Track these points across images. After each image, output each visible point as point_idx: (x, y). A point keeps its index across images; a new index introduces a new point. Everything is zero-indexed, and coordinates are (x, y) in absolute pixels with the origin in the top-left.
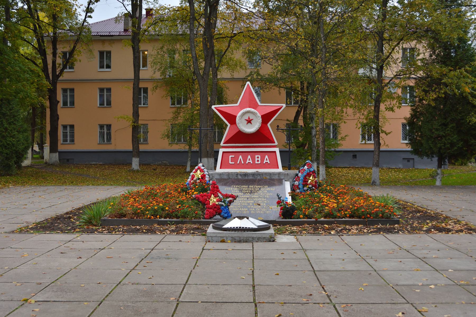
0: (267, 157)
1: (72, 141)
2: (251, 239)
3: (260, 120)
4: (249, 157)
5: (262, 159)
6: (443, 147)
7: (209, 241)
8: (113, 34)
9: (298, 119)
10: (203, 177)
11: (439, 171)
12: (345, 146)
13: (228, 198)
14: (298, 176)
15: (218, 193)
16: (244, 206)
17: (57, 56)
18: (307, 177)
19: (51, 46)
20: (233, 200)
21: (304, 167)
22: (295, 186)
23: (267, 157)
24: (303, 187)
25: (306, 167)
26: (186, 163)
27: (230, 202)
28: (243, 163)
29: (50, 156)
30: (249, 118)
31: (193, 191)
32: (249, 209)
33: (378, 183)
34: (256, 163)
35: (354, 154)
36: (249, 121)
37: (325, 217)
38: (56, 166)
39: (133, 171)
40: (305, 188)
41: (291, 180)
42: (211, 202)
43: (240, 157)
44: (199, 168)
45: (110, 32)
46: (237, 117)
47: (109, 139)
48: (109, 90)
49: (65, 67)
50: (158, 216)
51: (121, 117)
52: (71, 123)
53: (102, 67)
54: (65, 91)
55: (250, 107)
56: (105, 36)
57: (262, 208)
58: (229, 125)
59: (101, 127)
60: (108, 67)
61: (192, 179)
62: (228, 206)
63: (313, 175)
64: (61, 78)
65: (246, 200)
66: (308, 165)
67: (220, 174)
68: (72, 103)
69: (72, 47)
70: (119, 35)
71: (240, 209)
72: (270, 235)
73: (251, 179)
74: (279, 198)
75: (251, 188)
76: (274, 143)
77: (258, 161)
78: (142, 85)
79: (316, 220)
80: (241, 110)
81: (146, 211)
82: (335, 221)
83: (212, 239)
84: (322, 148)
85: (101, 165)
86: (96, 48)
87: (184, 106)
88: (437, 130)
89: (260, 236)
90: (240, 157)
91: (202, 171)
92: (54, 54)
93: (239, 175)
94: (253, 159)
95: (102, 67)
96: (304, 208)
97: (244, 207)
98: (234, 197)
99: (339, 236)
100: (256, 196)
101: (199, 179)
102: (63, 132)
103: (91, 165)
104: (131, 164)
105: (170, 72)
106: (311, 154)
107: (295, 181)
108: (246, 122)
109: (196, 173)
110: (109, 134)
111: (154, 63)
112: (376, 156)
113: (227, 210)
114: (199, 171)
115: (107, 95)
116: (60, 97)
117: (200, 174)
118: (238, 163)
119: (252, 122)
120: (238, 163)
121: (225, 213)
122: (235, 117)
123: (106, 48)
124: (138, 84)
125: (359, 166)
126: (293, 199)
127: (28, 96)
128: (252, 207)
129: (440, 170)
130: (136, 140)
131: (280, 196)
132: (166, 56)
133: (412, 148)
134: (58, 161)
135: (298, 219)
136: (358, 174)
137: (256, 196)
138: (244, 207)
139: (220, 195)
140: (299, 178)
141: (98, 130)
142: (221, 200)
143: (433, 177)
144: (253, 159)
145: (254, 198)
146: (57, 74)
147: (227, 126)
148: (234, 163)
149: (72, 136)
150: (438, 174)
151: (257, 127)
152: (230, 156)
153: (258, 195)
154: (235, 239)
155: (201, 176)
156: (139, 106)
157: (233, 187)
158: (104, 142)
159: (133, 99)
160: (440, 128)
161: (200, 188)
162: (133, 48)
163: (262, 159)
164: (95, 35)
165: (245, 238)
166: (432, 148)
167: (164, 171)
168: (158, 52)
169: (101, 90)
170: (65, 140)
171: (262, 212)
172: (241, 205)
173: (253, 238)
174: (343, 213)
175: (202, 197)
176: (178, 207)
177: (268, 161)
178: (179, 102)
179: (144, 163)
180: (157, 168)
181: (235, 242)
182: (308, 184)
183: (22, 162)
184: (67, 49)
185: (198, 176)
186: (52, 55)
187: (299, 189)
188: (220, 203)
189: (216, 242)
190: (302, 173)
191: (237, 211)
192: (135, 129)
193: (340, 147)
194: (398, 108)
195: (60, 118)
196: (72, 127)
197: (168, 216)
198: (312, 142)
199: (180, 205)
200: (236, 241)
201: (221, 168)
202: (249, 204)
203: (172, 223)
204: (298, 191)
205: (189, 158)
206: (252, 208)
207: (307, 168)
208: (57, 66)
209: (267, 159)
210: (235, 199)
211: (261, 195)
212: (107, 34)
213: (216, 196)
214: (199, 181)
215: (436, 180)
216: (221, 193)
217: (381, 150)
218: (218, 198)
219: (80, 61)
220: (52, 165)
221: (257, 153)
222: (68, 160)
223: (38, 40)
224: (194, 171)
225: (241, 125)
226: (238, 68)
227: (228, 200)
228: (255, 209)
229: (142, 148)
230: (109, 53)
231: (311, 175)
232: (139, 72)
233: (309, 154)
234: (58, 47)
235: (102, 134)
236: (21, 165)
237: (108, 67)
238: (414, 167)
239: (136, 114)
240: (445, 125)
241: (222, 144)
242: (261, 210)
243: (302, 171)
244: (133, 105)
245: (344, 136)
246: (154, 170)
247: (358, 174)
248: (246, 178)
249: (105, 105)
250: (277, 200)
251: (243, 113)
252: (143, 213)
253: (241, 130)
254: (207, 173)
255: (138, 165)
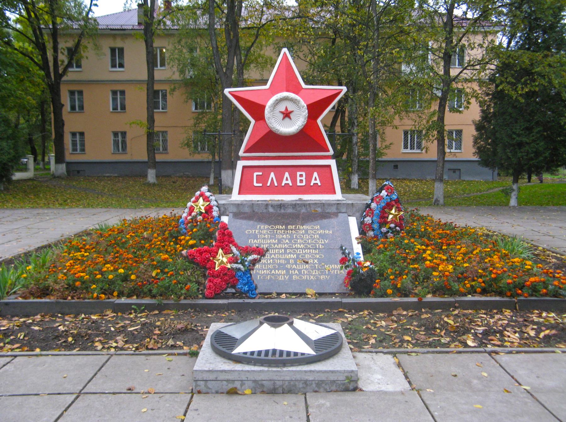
0: (315, 175)
1: (83, 150)
2: (301, 386)
3: (305, 113)
4: (287, 175)
5: (309, 179)
6: (525, 157)
7: (199, 392)
8: (126, 27)
9: (335, 125)
10: (209, 209)
11: (515, 187)
12: (389, 155)
13: (250, 255)
14: (370, 209)
15: (231, 245)
16: (279, 265)
17: (59, 51)
18: (386, 210)
19: (51, 41)
20: (260, 258)
21: (381, 192)
22: (366, 225)
23: (315, 175)
24: (380, 227)
25: (384, 193)
26: (210, 174)
27: (254, 262)
28: (276, 184)
29: (55, 167)
30: (286, 109)
31: (188, 238)
32: (288, 270)
33: (441, 201)
34: (299, 184)
35: (396, 164)
36: (287, 115)
37: (434, 293)
38: (63, 179)
39: (150, 185)
40: (384, 230)
41: (358, 214)
42: (217, 263)
43: (272, 175)
44: (202, 195)
45: (121, 26)
46: (267, 108)
47: (124, 148)
48: (123, 93)
49: (70, 65)
50: (115, 294)
51: (133, 123)
52: (81, 130)
53: (114, 66)
54: (72, 93)
55: (288, 91)
56: (116, 30)
57: (312, 270)
58: (253, 121)
59: (116, 134)
60: (121, 66)
61: (190, 214)
62: (250, 270)
63: (396, 206)
64: (64, 78)
65: (282, 254)
66: (388, 189)
67: (238, 204)
68: (82, 108)
69: (76, 41)
70: (132, 29)
71: (273, 272)
72: (346, 374)
73: (290, 214)
74: (344, 253)
75: (292, 230)
76: (329, 151)
77: (301, 181)
78: (156, 87)
79: (420, 300)
80: (273, 95)
81: (91, 282)
82: (456, 302)
83: (206, 386)
84: (373, 159)
85: (116, 177)
86: (106, 45)
87: (208, 111)
88: (519, 135)
89: (324, 378)
90: (272, 175)
91: (206, 199)
92: (55, 49)
93: (270, 207)
94: (294, 179)
95: (114, 66)
96: (392, 274)
97: (281, 267)
98: (261, 252)
99: (490, 353)
100: (300, 244)
101: (201, 213)
102: (73, 141)
103: (104, 177)
104: (146, 176)
105: (190, 73)
106: (351, 165)
107: (365, 217)
108: (281, 116)
109: (197, 203)
110: (124, 143)
111: (171, 59)
112: (440, 169)
113: (248, 278)
114: (201, 200)
115: (120, 98)
116: (65, 99)
117: (203, 205)
118: (268, 185)
119: (291, 115)
120: (268, 185)
121: (245, 285)
122: (263, 107)
123: (119, 44)
124: (153, 87)
125: (401, 178)
126: (366, 250)
127: (13, 95)
128: (294, 266)
129: (515, 185)
130: (151, 149)
131: (347, 251)
132: (184, 51)
133: (480, 158)
134: (66, 173)
135: (382, 296)
136: (402, 187)
137: (300, 244)
138: (281, 267)
139: (234, 249)
140: (372, 211)
141: (112, 138)
142: (237, 260)
143: (507, 193)
144: (294, 179)
145: (297, 249)
146: (60, 72)
147: (250, 122)
148: (261, 185)
149: (83, 145)
150: (513, 190)
151: (301, 124)
152: (255, 174)
153: (303, 244)
154: (263, 385)
155: (205, 209)
156: (155, 111)
157: (260, 227)
158: (119, 151)
159: (147, 102)
160: (523, 132)
161: (201, 233)
162: (146, 41)
163: (309, 179)
164: (104, 29)
165: (287, 383)
166: (510, 158)
167: (185, 184)
168: (175, 47)
169: (114, 93)
170: (75, 149)
171: (312, 277)
172: (274, 262)
173: (306, 382)
174: (468, 285)
175: (201, 254)
176: (154, 274)
177: (318, 182)
178: (202, 107)
179: (164, 174)
180: (177, 180)
181: (263, 392)
182: (388, 223)
183: (12, 174)
184: (71, 44)
185: (200, 208)
186: (52, 50)
187: (373, 230)
188: (235, 266)
189: (217, 392)
190: (377, 203)
191: (267, 275)
192: (151, 136)
193: (383, 157)
194: (465, 108)
195: (66, 123)
196: (82, 134)
197: (135, 292)
198: (353, 151)
199: (159, 271)
200: (265, 389)
201: (239, 193)
202: (288, 260)
203: (140, 308)
204: (371, 233)
205: (213, 170)
206: (294, 269)
207: (386, 194)
208: (60, 63)
209: (316, 179)
210: (264, 255)
211: (308, 243)
212: (119, 27)
213: (227, 251)
214: (201, 217)
215: (511, 197)
216: (236, 245)
217: (446, 159)
218: (231, 255)
219: (87, 58)
220: (58, 177)
221: (299, 168)
222: (78, 172)
223: (34, 31)
224: (193, 199)
225: (273, 121)
226: (269, 66)
227: (250, 258)
228: (299, 270)
229: (159, 158)
230: (121, 50)
231: (393, 206)
232: (153, 73)
233: (349, 165)
234: (59, 40)
235: (116, 143)
236: (11, 179)
237: (121, 66)
238: (460, 178)
239: (151, 120)
240: (529, 129)
241: (241, 153)
242: (310, 274)
243: (378, 200)
244: (148, 108)
245: (388, 144)
246: (174, 182)
247: (402, 187)
248: (282, 211)
249: (119, 110)
250: (340, 256)
251: (277, 100)
252: (87, 288)
253: (273, 130)
254: (215, 203)
255: (155, 176)
